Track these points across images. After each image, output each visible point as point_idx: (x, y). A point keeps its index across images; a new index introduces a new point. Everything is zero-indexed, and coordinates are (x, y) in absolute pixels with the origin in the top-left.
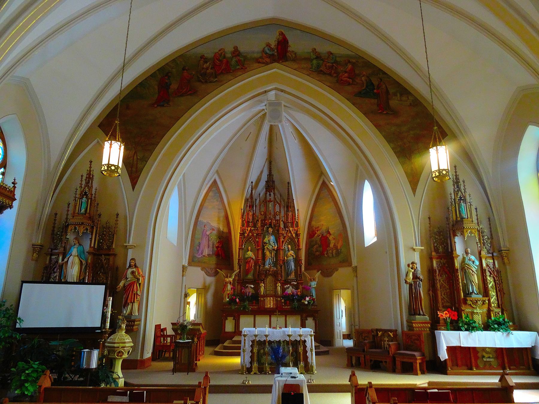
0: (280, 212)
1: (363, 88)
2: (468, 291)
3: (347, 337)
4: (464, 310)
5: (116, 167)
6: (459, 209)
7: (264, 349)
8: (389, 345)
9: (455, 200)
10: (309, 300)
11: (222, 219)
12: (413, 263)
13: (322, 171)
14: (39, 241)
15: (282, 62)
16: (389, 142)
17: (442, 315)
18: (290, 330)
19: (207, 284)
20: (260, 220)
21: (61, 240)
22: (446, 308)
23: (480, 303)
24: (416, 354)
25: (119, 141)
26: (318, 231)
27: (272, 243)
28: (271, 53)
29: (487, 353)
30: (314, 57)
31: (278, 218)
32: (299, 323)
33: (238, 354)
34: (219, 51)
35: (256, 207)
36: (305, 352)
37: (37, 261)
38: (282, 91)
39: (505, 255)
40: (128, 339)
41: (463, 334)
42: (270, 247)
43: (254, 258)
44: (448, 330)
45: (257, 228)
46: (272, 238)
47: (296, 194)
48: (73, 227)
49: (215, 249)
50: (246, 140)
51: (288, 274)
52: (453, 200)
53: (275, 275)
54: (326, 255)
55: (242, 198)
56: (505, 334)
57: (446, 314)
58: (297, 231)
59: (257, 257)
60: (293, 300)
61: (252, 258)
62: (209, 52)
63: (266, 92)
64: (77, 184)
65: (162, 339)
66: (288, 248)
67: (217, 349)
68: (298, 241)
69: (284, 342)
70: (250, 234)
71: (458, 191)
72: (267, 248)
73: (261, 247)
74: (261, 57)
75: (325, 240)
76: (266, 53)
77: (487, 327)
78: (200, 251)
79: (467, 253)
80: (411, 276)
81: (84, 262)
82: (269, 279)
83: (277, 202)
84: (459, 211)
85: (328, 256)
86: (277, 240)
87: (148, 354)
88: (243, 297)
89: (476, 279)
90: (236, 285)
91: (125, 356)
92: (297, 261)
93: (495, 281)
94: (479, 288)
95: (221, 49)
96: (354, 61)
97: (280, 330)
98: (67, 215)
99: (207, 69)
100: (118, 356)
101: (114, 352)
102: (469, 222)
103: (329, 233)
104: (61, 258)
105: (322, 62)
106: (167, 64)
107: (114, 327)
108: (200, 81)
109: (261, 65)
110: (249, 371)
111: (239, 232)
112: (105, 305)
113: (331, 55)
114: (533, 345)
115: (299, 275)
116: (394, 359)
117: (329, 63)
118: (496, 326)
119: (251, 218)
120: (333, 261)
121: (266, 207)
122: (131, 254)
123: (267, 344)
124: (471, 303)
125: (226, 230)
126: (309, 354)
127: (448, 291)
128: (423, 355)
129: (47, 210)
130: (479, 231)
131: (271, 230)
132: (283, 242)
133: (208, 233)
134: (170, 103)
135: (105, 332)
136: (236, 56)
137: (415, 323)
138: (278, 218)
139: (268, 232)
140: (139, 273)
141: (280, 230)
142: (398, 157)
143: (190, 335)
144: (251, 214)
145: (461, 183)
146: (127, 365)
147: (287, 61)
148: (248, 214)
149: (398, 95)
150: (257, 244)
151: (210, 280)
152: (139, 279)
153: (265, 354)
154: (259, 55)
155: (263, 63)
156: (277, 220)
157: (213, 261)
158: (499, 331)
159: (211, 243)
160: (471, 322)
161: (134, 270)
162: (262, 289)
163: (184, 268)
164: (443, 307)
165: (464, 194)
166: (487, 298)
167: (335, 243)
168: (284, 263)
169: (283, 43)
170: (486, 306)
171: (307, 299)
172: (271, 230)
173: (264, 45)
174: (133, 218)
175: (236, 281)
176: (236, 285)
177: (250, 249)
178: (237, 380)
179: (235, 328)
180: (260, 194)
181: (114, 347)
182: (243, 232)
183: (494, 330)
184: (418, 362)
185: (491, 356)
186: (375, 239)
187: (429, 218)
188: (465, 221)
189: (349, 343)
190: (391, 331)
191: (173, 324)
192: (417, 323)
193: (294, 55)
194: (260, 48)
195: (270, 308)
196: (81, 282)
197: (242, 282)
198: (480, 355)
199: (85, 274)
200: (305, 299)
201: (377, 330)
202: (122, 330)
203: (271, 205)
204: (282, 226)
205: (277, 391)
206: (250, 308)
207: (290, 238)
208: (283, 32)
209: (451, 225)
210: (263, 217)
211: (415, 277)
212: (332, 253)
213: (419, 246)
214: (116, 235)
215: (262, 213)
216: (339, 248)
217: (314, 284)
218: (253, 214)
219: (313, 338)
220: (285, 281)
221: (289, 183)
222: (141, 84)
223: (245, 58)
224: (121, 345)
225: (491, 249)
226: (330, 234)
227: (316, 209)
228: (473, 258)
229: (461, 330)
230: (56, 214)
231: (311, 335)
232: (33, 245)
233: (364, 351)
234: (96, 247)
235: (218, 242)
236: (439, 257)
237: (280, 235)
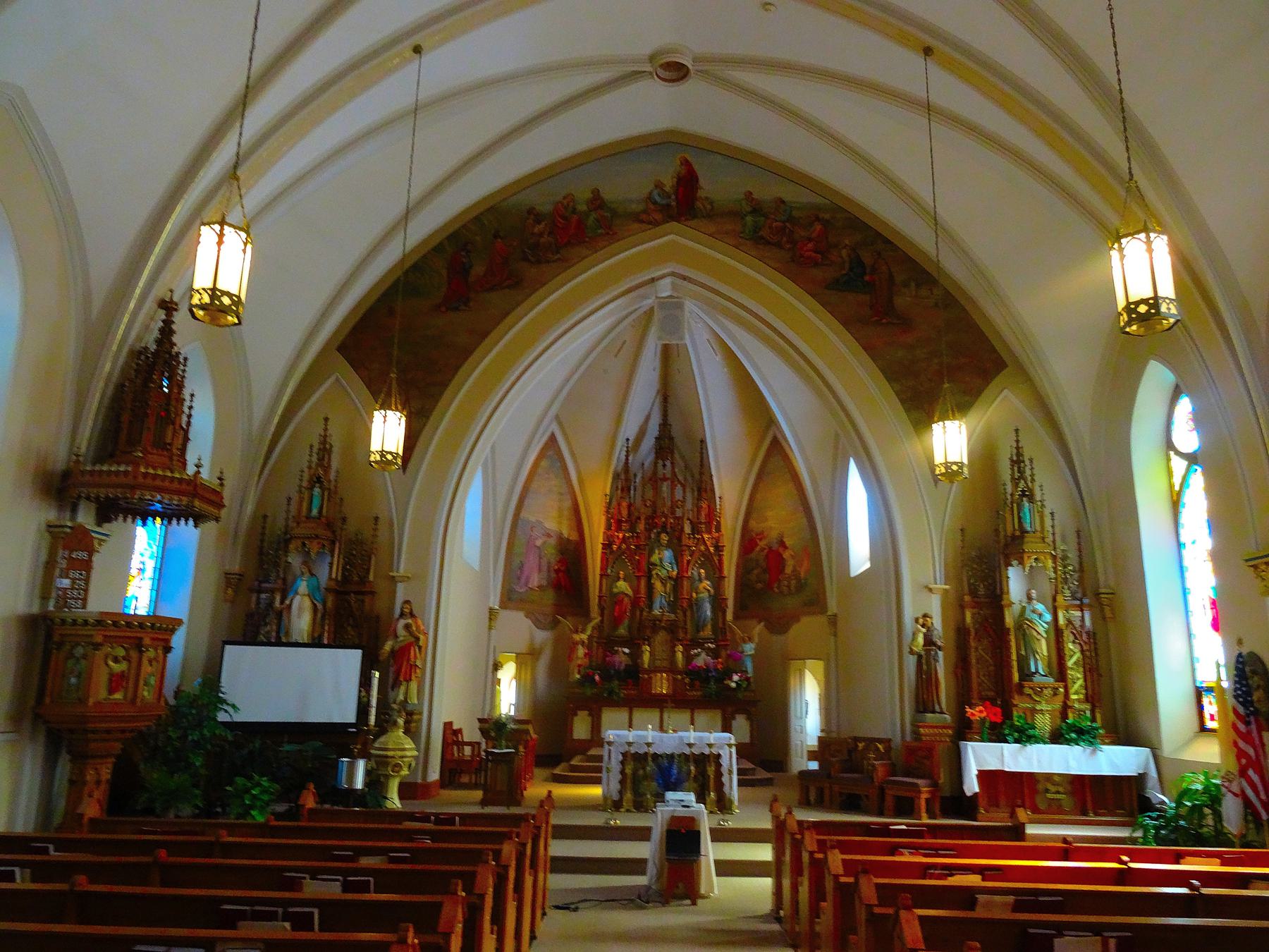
0: (684, 501)
1: (844, 272)
2: (1029, 668)
3: (812, 756)
4: (1016, 706)
5: (1151, 301)
6: (1019, 513)
7: (644, 768)
8: (873, 766)
9: (1012, 495)
10: (740, 680)
11: (566, 513)
12: (925, 616)
13: (771, 418)
14: (236, 568)
15: (686, 220)
16: (889, 380)
17: (973, 714)
18: (692, 736)
19: (537, 646)
20: (642, 518)
21: (276, 565)
22: (983, 699)
23: (1048, 692)
24: (919, 782)
25: (397, 409)
26: (761, 540)
27: (666, 564)
28: (664, 202)
29: (1055, 784)
30: (749, 209)
31: (679, 513)
32: (719, 723)
33: (597, 781)
34: (564, 198)
35: (635, 490)
36: (719, 774)
37: (233, 602)
38: (684, 278)
39: (1105, 602)
40: (408, 744)
41: (1009, 749)
42: (663, 573)
43: (630, 592)
44: (982, 741)
45: (637, 533)
46: (667, 554)
47: (716, 462)
48: (299, 542)
49: (553, 575)
50: (616, 356)
51: (699, 628)
52: (1009, 497)
53: (672, 628)
54: (776, 590)
55: (608, 471)
56: (1089, 749)
57: (981, 712)
58: (718, 540)
59: (636, 591)
60: (707, 680)
61: (626, 595)
62: (543, 200)
63: (653, 280)
64: (303, 460)
65: (455, 748)
66: (699, 574)
67: (557, 771)
68: (721, 561)
69: (680, 756)
70: (624, 546)
71: (1019, 478)
72: (657, 574)
73: (645, 572)
74: (645, 212)
75: (775, 558)
76: (655, 203)
77: (1057, 737)
78: (523, 580)
79: (1030, 598)
80: (920, 640)
81: (320, 606)
82: (661, 637)
83: (678, 480)
84: (1020, 518)
85: (781, 592)
86: (678, 558)
87: (434, 775)
88: (608, 673)
89: (1043, 648)
90: (595, 648)
91: (405, 772)
92: (718, 601)
93: (1082, 651)
94: (1049, 665)
95: (568, 195)
96: (827, 216)
97: (675, 735)
98: (287, 519)
99: (541, 234)
100: (393, 771)
101: (387, 764)
102: (1037, 540)
103: (782, 544)
104: (278, 599)
105: (763, 218)
106: (464, 226)
107: (385, 725)
108: (526, 259)
109: (644, 226)
110: (617, 806)
111: (601, 540)
112: (365, 683)
113: (782, 205)
114: (1141, 772)
115: (720, 630)
116: (882, 790)
117: (777, 221)
118: (1073, 735)
119: (625, 513)
120: (791, 603)
121: (656, 490)
122: (401, 593)
123: (650, 759)
124: (1030, 692)
125: (574, 536)
126: (725, 779)
127: (992, 668)
128: (935, 785)
129: (250, 508)
130: (1054, 558)
131: (664, 537)
132: (689, 562)
133: (539, 543)
134: (471, 304)
135: (368, 732)
136: (595, 209)
137: (923, 727)
138: (679, 513)
139: (659, 541)
140: (418, 627)
141: (684, 537)
142: (907, 410)
143: (510, 741)
144: (624, 504)
145: (1027, 462)
146: (407, 791)
147: (694, 217)
148: (619, 505)
149: (913, 284)
150: (638, 566)
151: (542, 636)
152: (418, 639)
153: (646, 777)
154: (641, 207)
155: (650, 223)
156: (678, 518)
157: (549, 597)
158: (1078, 745)
159: (544, 562)
160: (1026, 726)
161: (410, 621)
162: (646, 657)
163: (492, 614)
164: (981, 698)
165: (1030, 484)
166: (1061, 684)
167: (794, 567)
168: (691, 606)
169: (688, 181)
170: (1060, 698)
171: (736, 678)
172: (664, 537)
173: (652, 186)
174: (404, 524)
175: (595, 639)
176: (595, 648)
177: (621, 576)
178: (596, 820)
179: (592, 731)
180: (643, 464)
181: (387, 757)
182: (609, 541)
183: (1068, 742)
184: (924, 796)
185: (1061, 789)
186: (867, 565)
187: (961, 530)
188: (1028, 538)
189: (814, 765)
190: (880, 741)
191: (480, 720)
192: (927, 727)
193: (709, 207)
194: (645, 192)
195: (661, 695)
196: (315, 643)
197: (605, 642)
198: (1040, 787)
199: (323, 626)
200: (731, 679)
201: (857, 740)
202: (399, 728)
203: (665, 487)
204: (687, 529)
205: (657, 833)
206: (623, 693)
207: (703, 555)
208: (689, 159)
209: (1002, 544)
210: (649, 511)
211: (929, 641)
212: (788, 587)
213: (941, 584)
214: (375, 556)
215: (648, 503)
216: (802, 575)
217: (749, 648)
218: (630, 506)
219: (734, 750)
220: (691, 640)
221: (703, 442)
222: (416, 267)
223: (615, 213)
224: (400, 753)
225: (1080, 591)
226: (785, 547)
227: (758, 496)
228: (1040, 607)
229: (1006, 742)
230: (265, 517)
231: (730, 746)
232: (226, 574)
233: (829, 776)
234: (339, 578)
235: (559, 562)
236: (977, 605)
237: (685, 548)
